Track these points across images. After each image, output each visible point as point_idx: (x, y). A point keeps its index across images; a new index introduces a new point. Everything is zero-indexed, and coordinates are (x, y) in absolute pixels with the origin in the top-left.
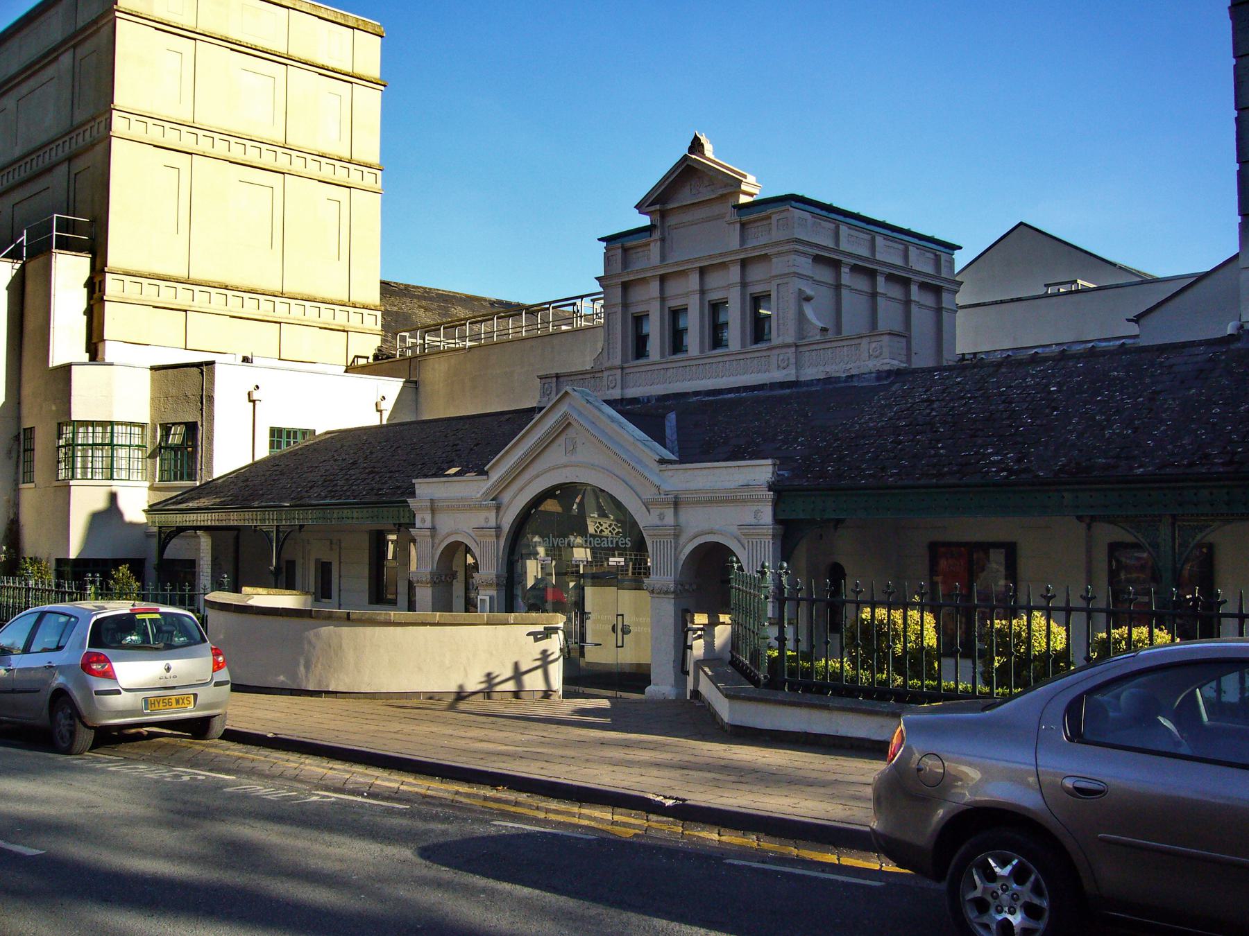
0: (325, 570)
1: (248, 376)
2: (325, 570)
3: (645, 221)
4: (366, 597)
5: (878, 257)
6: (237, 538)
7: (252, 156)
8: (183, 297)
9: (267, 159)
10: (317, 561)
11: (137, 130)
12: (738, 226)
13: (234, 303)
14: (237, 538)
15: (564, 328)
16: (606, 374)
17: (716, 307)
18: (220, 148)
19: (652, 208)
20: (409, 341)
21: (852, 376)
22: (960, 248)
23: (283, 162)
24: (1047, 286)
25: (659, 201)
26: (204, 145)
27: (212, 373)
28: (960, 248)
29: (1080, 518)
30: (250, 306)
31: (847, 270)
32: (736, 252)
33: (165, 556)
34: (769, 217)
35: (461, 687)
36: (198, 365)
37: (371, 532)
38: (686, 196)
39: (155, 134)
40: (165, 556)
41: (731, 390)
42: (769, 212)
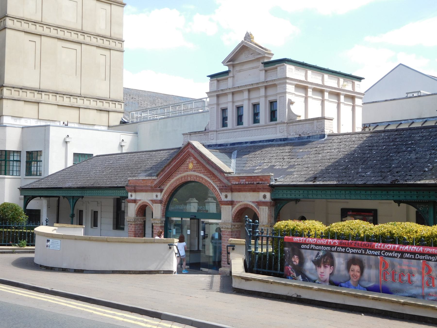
0: (95, 214)
1: (66, 131)
2: (95, 214)
3: (226, 69)
4: (111, 227)
5: (326, 84)
6: (59, 199)
7: (67, 35)
8: (37, 97)
9: (74, 37)
10: (92, 210)
11: (17, 25)
12: (264, 71)
13: (59, 100)
14: (59, 199)
15: (200, 111)
16: (210, 133)
17: (239, 108)
18: (53, 33)
19: (229, 63)
20: (135, 115)
21: (309, 137)
22: (363, 78)
23: (81, 38)
24: (407, 93)
25: (233, 60)
26: (46, 31)
27: (49, 130)
28: (363, 78)
29: (395, 201)
30: (66, 101)
31: (311, 90)
32: (263, 82)
33: (27, 208)
34: (276, 68)
35: (296, 203)
36: (45, 126)
37: (114, 199)
38: (243, 58)
39: (25, 27)
40: (27, 208)
41: (260, 141)
42: (277, 65)
